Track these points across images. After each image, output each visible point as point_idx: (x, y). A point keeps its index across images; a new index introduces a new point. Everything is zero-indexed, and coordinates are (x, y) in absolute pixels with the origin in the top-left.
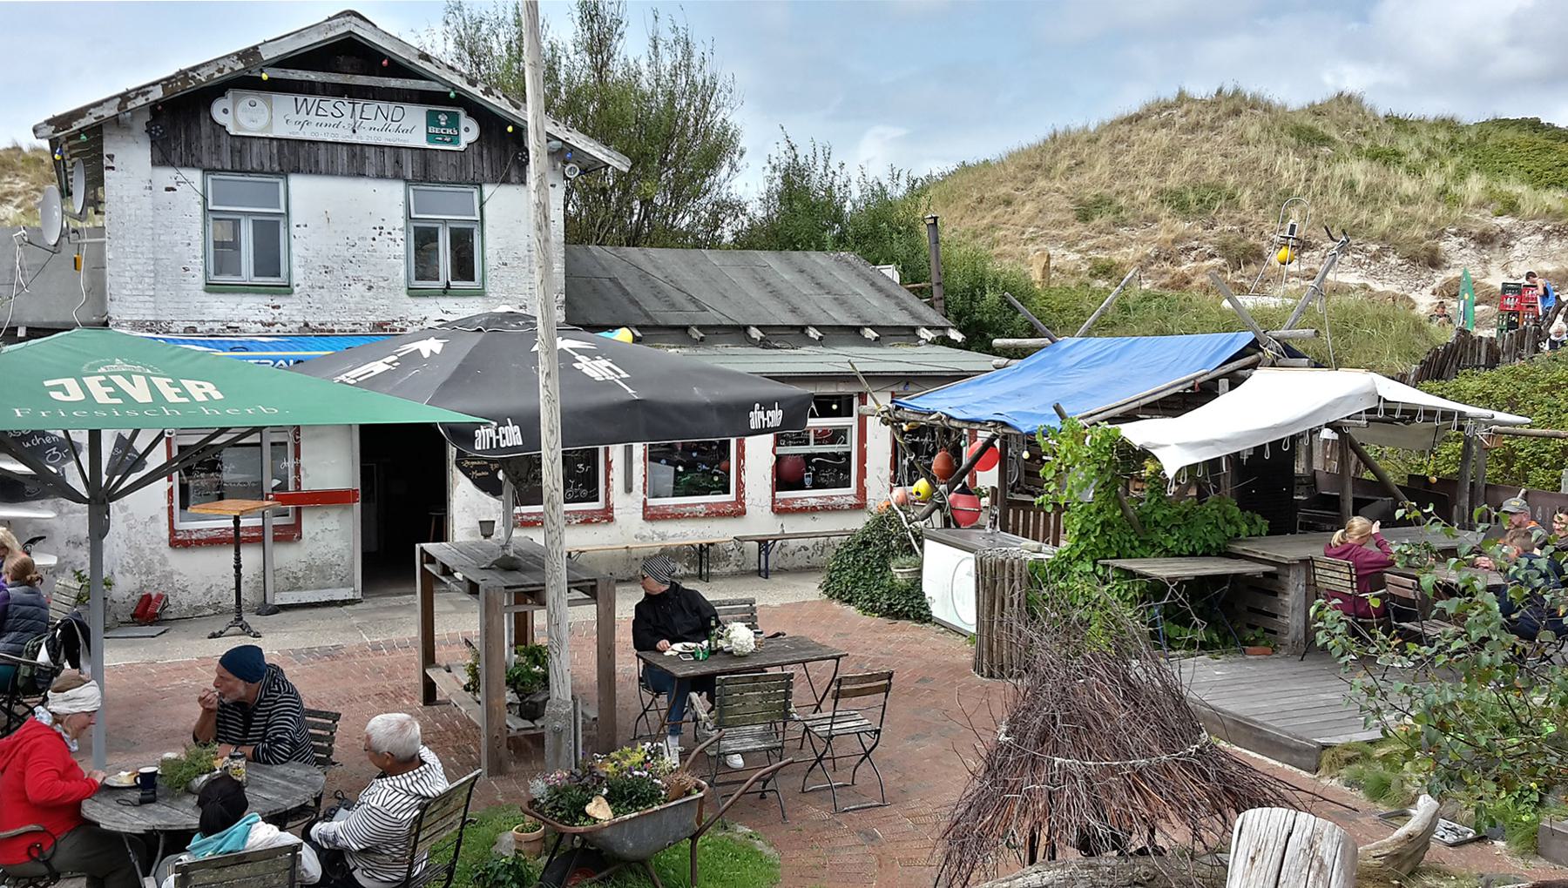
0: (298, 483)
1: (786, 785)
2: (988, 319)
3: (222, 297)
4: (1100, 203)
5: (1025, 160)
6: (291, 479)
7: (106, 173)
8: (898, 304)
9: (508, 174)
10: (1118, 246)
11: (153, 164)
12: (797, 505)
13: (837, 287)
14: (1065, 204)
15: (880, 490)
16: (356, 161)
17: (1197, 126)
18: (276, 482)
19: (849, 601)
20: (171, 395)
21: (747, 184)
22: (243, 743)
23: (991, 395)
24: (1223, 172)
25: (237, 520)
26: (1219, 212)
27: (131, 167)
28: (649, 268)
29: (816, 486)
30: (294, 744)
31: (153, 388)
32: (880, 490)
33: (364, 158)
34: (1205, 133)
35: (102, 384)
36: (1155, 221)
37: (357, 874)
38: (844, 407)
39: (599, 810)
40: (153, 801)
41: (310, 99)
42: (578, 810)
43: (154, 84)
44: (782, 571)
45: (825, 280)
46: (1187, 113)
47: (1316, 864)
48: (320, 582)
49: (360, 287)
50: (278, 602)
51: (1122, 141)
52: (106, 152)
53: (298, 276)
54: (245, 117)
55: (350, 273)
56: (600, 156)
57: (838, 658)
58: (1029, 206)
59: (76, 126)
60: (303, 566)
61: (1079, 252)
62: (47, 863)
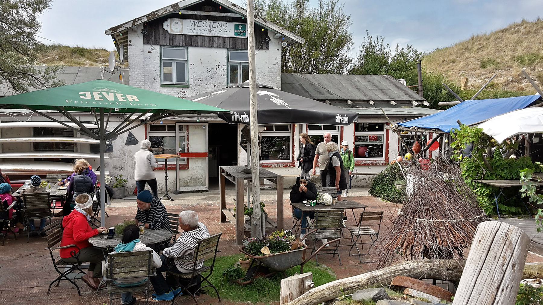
0: (188, 150)
1: (342, 253)
2: (437, 97)
3: (166, 89)
4: (490, 61)
5: (461, 47)
6: (186, 148)
7: (129, 47)
8: (405, 93)
9: (262, 46)
10: (496, 77)
11: (144, 44)
12: (362, 163)
13: (382, 87)
14: (477, 62)
15: (394, 157)
16: (211, 42)
17: (529, 32)
18: (180, 149)
19: (379, 197)
20: (121, 99)
21: (353, 54)
22: (146, 223)
23: (433, 120)
24: (539, 49)
25: (166, 161)
26: (537, 64)
27: (137, 43)
28: (313, 81)
29: (370, 156)
30: (162, 223)
31: (115, 97)
32: (394, 157)
33: (213, 41)
34: (532, 35)
35: (98, 94)
36: (511, 68)
37: (177, 266)
38: (381, 128)
39: (266, 251)
40: (112, 238)
41: (196, 21)
42: (258, 251)
43: (144, 16)
44: (356, 187)
45: (378, 84)
46: (525, 28)
47: (508, 243)
48: (195, 184)
49: (211, 86)
50: (181, 190)
51: (499, 39)
52: (129, 40)
53: (191, 82)
54: (174, 27)
55: (208, 81)
56: (294, 39)
57: (364, 208)
58: (462, 63)
59: (119, 30)
60: (189, 178)
61: (481, 79)
62: (77, 258)
